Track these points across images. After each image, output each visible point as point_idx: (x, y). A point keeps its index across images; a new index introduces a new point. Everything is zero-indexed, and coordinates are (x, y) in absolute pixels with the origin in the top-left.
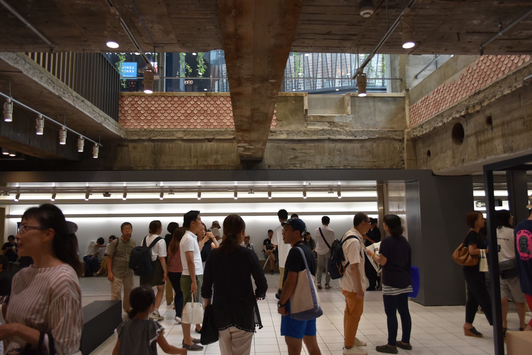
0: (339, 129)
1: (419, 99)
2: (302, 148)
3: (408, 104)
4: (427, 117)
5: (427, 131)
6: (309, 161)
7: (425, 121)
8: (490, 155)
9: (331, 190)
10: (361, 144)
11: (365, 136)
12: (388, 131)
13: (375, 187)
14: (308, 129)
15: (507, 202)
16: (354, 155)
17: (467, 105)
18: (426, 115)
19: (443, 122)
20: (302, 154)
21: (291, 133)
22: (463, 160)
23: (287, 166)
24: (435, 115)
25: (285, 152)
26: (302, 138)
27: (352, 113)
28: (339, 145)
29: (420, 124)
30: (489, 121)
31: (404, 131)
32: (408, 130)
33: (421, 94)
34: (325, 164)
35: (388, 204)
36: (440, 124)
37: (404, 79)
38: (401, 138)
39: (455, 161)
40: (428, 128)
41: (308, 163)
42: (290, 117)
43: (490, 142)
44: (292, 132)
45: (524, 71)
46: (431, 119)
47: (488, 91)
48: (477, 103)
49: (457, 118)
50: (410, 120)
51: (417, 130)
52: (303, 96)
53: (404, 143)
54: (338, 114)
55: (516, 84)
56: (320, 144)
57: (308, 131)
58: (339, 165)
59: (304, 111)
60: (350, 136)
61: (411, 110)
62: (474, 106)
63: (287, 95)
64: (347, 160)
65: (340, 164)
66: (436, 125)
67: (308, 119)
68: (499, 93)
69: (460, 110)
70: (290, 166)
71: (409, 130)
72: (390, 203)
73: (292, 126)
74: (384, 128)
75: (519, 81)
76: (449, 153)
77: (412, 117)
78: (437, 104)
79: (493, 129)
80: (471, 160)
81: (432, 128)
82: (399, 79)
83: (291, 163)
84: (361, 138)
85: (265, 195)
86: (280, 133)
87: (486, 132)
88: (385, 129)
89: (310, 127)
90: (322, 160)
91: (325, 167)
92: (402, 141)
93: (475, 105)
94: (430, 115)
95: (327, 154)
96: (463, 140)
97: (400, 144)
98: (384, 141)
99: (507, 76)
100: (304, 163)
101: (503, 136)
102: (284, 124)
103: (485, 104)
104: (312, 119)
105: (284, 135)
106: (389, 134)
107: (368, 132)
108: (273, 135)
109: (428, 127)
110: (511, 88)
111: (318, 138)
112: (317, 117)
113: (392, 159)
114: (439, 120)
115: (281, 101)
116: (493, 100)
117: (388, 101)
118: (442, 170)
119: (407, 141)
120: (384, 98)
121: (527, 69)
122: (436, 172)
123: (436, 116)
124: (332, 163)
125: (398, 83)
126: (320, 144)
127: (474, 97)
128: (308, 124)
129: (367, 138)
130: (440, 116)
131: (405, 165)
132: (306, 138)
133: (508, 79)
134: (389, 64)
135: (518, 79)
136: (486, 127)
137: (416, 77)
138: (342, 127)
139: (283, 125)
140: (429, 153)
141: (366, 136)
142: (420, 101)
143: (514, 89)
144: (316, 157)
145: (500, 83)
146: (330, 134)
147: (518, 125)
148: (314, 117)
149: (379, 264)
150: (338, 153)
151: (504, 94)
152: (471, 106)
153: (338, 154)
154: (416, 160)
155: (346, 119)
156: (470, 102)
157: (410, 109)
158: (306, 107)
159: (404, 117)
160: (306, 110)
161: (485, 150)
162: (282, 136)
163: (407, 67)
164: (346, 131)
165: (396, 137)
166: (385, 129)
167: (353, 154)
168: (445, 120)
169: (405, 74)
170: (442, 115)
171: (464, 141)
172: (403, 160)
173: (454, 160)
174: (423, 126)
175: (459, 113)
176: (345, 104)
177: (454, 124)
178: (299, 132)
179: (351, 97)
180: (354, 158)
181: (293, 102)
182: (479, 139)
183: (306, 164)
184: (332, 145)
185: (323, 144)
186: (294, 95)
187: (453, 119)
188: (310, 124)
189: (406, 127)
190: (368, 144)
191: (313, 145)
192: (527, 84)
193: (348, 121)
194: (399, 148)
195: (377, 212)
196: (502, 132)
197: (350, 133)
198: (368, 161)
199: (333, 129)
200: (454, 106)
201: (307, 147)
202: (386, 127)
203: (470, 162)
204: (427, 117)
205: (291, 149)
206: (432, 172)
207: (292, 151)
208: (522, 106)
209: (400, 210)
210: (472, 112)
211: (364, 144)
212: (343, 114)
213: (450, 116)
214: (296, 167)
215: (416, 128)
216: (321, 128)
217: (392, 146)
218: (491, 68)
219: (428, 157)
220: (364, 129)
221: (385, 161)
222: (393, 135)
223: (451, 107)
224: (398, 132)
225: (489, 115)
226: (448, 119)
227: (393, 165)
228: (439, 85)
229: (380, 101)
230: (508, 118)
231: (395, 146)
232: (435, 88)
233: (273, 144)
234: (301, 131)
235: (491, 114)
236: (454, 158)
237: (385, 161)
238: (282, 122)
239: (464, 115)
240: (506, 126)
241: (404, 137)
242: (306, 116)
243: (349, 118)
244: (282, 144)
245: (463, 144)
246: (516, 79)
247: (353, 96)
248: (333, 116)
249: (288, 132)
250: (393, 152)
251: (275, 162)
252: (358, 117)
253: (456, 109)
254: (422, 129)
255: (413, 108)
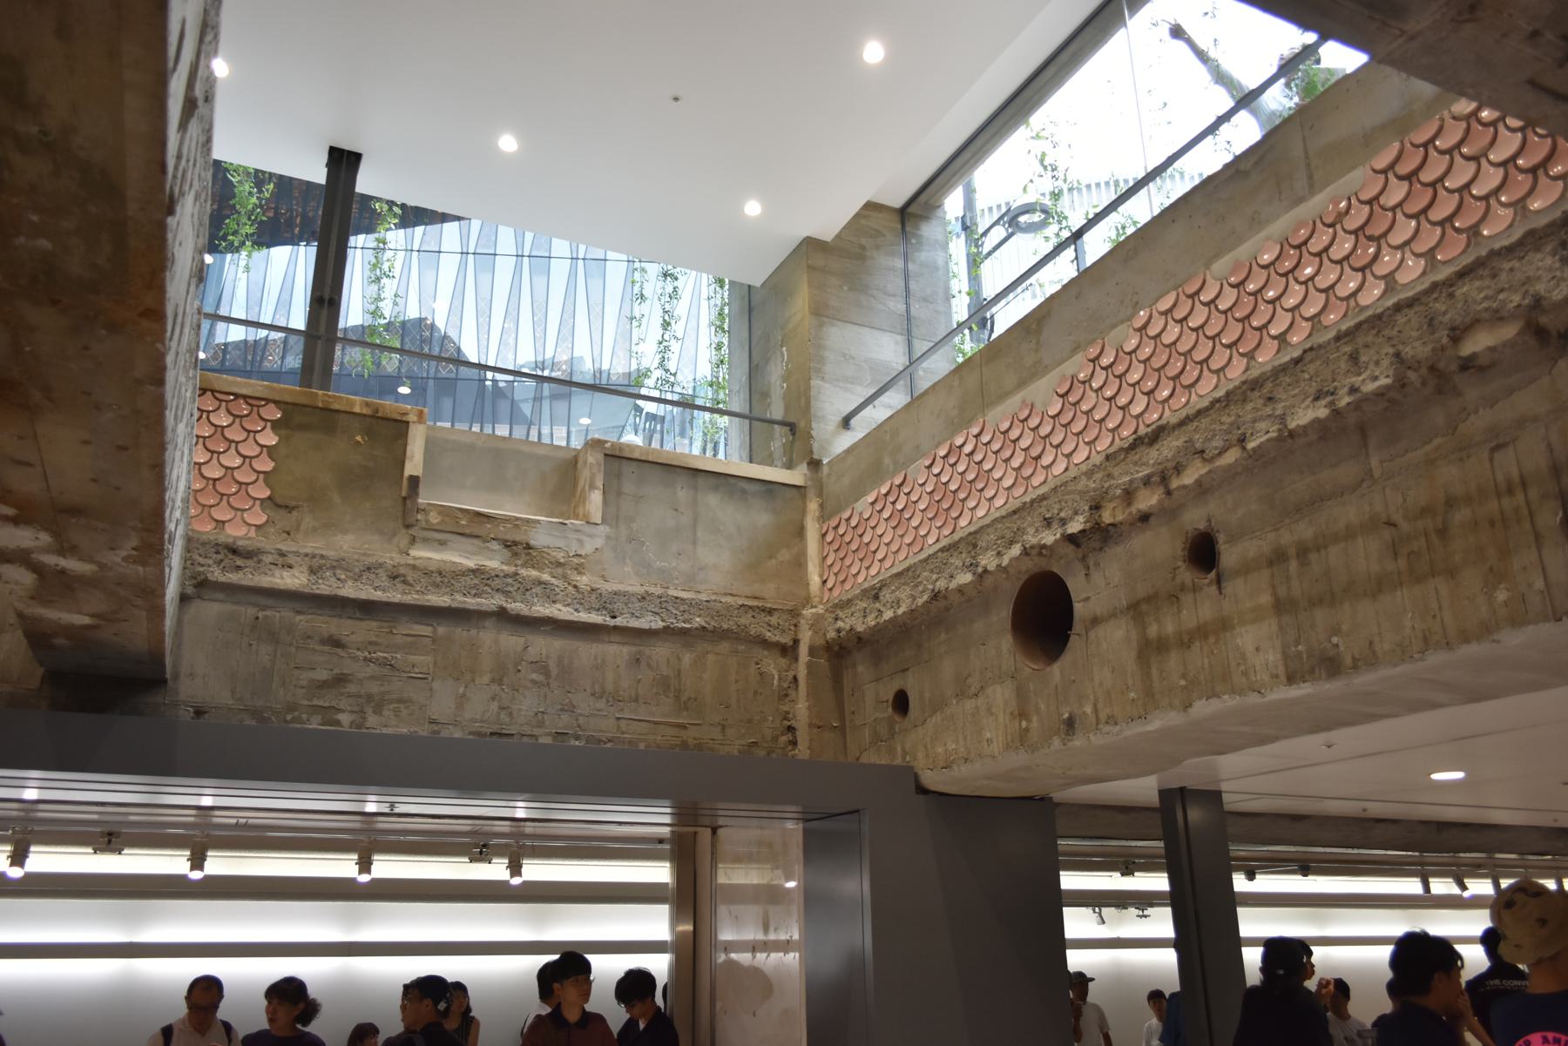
0: (546, 577)
1: (864, 494)
2: (374, 639)
3: (817, 514)
4: (901, 556)
5: (900, 612)
6: (400, 701)
7: (895, 571)
8: (1213, 694)
9: (484, 846)
10: (634, 649)
11: (650, 617)
12: (743, 605)
13: (661, 841)
14: (415, 558)
15: (1168, 910)
16: (604, 692)
17: (1095, 490)
18: (894, 548)
19: (980, 570)
20: (372, 669)
21: (334, 568)
22: (1070, 724)
23: (289, 717)
24: (939, 546)
25: (293, 650)
26: (378, 595)
27: (604, 521)
28: (543, 646)
29: (866, 585)
30: (1203, 552)
31: (799, 615)
32: (814, 610)
33: (875, 473)
34: (473, 720)
35: (713, 913)
36: (966, 578)
37: (802, 424)
38: (786, 639)
39: (1027, 730)
40: (903, 596)
41: (397, 712)
42: (336, 499)
43: (1212, 640)
44: (338, 565)
45: (1401, 319)
46: (920, 561)
47: (1205, 422)
48: (1147, 481)
49: (1044, 546)
50: (821, 576)
51: (853, 609)
52: (408, 423)
53: (796, 659)
54: (547, 517)
55: (1356, 380)
56: (460, 633)
57: (414, 567)
58: (536, 731)
59: (405, 482)
60: (589, 610)
61: (829, 538)
62: (1129, 495)
63: (336, 406)
64: (570, 709)
65: (541, 725)
66: (941, 584)
67: (419, 517)
68: (1262, 425)
69: (1063, 515)
70: (304, 716)
71: (820, 610)
72: (722, 910)
73: (339, 537)
74: (725, 594)
75: (1371, 366)
76: (1001, 695)
77: (829, 562)
78: (945, 502)
79: (1223, 585)
80: (1112, 720)
81: (925, 597)
82: (783, 423)
83: (315, 702)
84: (634, 624)
85: (174, 863)
86: (280, 560)
87: (1187, 599)
88: (729, 599)
89: (423, 554)
90: (462, 700)
91: (470, 733)
92: (788, 651)
93: (1137, 489)
94: (916, 548)
95: (486, 679)
96: (1069, 635)
97: (783, 662)
98: (725, 647)
99: (1305, 351)
100: (378, 710)
101: (1282, 606)
102: (302, 527)
103: (1188, 478)
104: (434, 518)
105: (295, 571)
106: (744, 620)
107: (664, 603)
108: (239, 568)
109: (904, 593)
110: (1329, 399)
111: (455, 605)
112: (459, 515)
113: (750, 721)
114: (956, 562)
115: (303, 427)
116: (1231, 456)
117: (744, 492)
118: (962, 770)
119: (812, 651)
120: (732, 481)
121: (1417, 308)
122: (932, 780)
123: (942, 550)
124: (504, 717)
125: (780, 437)
126: (459, 630)
127: (1134, 457)
128: (413, 540)
129: (661, 624)
130: (961, 546)
131: (800, 747)
132: (395, 596)
133: (1311, 361)
134: (745, 379)
135: (1363, 359)
136: (1187, 575)
137: (846, 422)
138: (560, 570)
139: (298, 529)
140: (901, 702)
141: (657, 618)
142: (870, 498)
143: (1344, 400)
144: (436, 685)
145: (1269, 385)
146: (507, 594)
147: (1366, 556)
148: (445, 511)
149: (214, 710)
150: (534, 676)
151: (1292, 425)
152: (1119, 492)
153: (534, 682)
154: (842, 729)
155: (580, 541)
156: (1109, 476)
157: (824, 535)
158: (414, 466)
159: (800, 562)
160: (414, 481)
161: (1184, 676)
162: (285, 574)
163: (815, 383)
164: (575, 587)
165: (769, 634)
166: (729, 599)
167: (597, 688)
168: (988, 561)
169: (807, 408)
170: (971, 542)
171: (1074, 641)
172: (791, 729)
173: (1024, 724)
174: (881, 594)
175: (1055, 525)
176: (581, 483)
177: (1024, 578)
178: (369, 569)
179: (605, 455)
180: (601, 704)
181: (359, 438)
182: (1153, 630)
183: (386, 713)
184: (511, 641)
185: (473, 632)
186: (365, 411)
187: (1026, 552)
188: (426, 540)
189: (807, 601)
190: (660, 652)
191: (425, 630)
192: (1412, 375)
193: (588, 549)
194: (780, 679)
195: (666, 942)
196: (1275, 594)
197: (593, 597)
198: (656, 723)
199: (523, 572)
200: (1033, 501)
201: (399, 640)
202: (734, 592)
203: (1107, 728)
204: (901, 556)
205: (323, 642)
206: (916, 776)
207: (326, 648)
208: (1377, 473)
209: (772, 937)
210: (1120, 518)
211: (647, 651)
212: (569, 518)
213: (1011, 543)
214: (338, 723)
215: (849, 602)
216: (470, 563)
217: (753, 667)
218: (988, 496)
219: (897, 718)
220: (652, 590)
221: (723, 728)
222: (757, 627)
223: (1014, 504)
224: (776, 615)
225: (1202, 526)
226: (999, 554)
227: (755, 743)
228: (955, 432)
229: (716, 489)
230: (1304, 531)
231: (763, 670)
232: (938, 445)
233: (234, 607)
234: (381, 565)
235: (1209, 521)
236: (1022, 714)
237: (723, 728)
238: (295, 513)
239: (1083, 532)
240: (1293, 565)
241: (800, 636)
242: (408, 502)
243: (591, 536)
244: (280, 615)
245: (1067, 658)
246: (1354, 358)
247: (617, 453)
248: (528, 521)
249: (316, 562)
250: (756, 693)
251: (233, 692)
252: (631, 540)
253: (1043, 510)
254: (877, 605)
255: (836, 528)
